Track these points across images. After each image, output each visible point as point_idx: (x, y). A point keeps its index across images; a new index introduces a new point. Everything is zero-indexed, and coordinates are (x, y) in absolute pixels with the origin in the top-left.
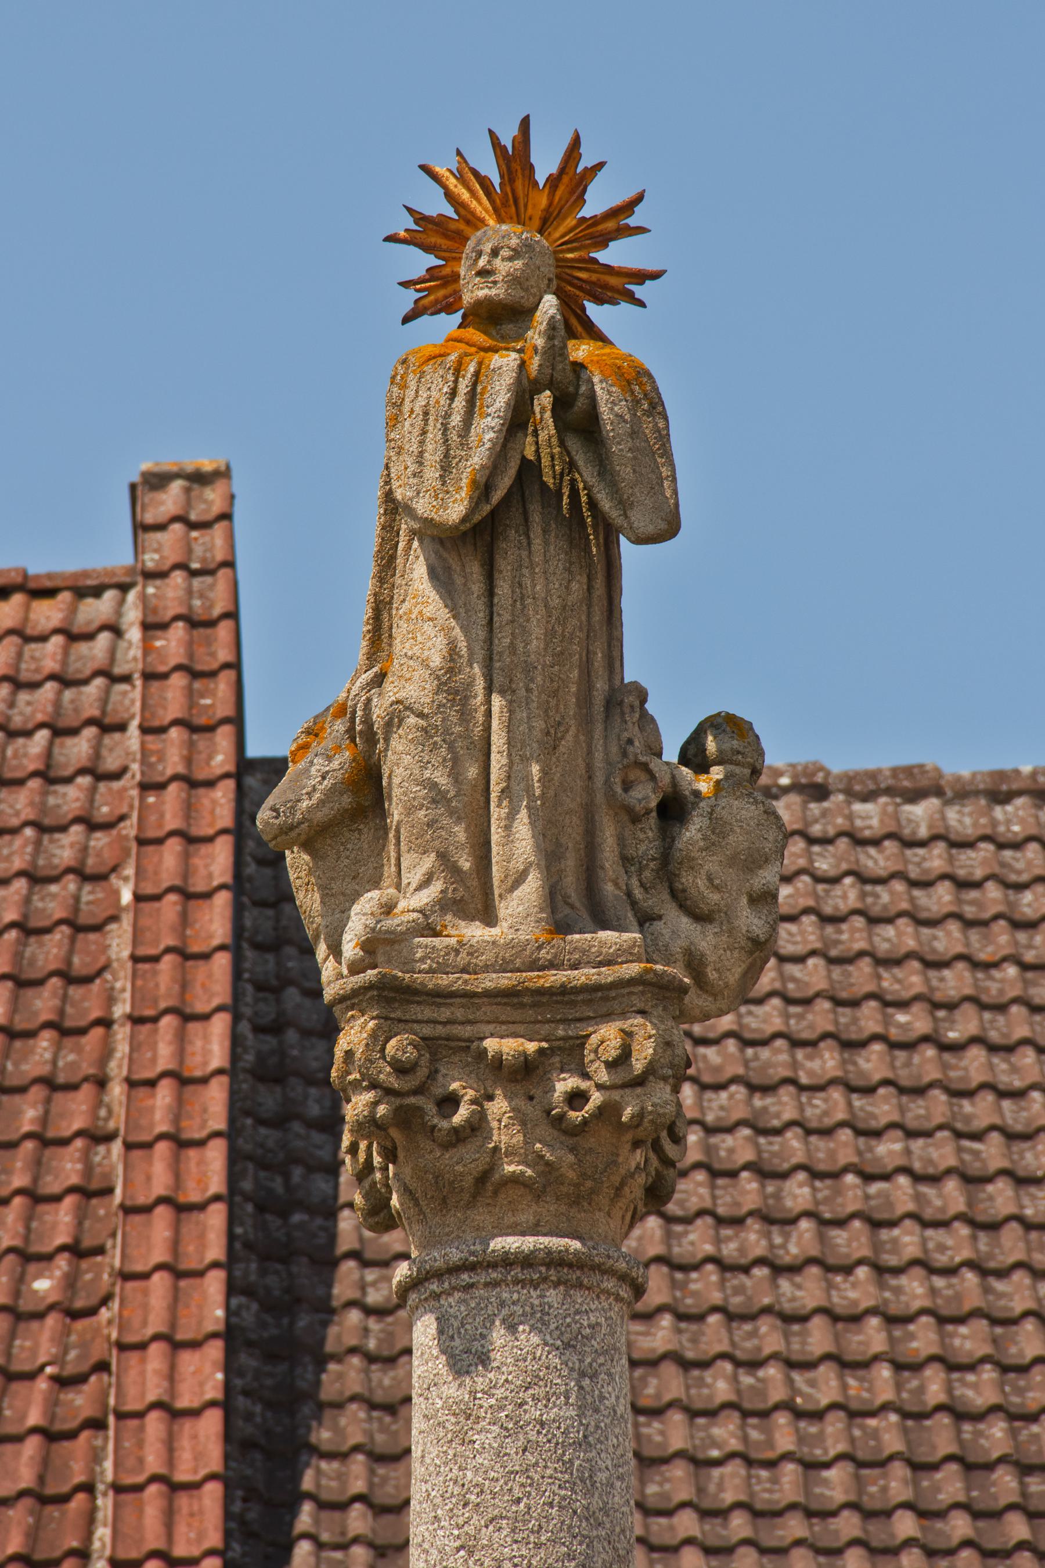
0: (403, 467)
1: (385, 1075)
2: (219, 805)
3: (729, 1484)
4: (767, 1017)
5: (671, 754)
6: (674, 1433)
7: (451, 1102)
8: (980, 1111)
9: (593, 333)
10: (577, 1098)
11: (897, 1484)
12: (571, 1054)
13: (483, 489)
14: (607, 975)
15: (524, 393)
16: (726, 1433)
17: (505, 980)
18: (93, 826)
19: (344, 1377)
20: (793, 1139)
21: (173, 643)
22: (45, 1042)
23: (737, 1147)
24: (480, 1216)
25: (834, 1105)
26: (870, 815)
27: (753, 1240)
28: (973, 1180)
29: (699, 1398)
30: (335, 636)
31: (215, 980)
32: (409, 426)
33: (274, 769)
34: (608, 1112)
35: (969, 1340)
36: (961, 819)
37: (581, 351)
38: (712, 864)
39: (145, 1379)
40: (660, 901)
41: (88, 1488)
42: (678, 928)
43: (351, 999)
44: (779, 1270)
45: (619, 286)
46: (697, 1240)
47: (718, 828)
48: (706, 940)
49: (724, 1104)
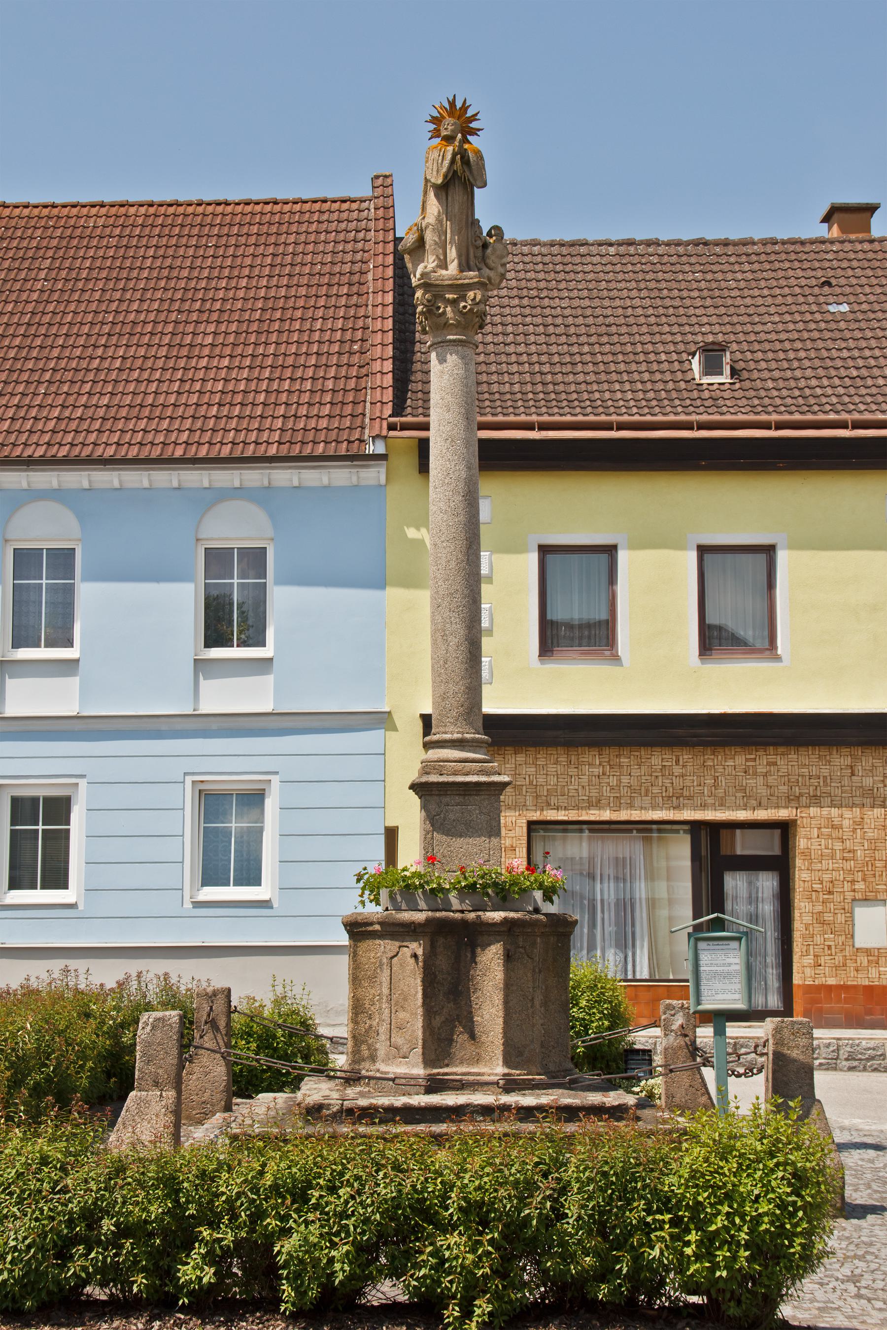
0: (429, 172)
1: (425, 302)
2: (390, 247)
3: (495, 388)
4: (504, 292)
5: (485, 234)
6: (484, 378)
7: (439, 308)
8: (547, 311)
9: (469, 142)
10: (465, 307)
11: (529, 387)
12: (463, 298)
13: (445, 176)
14: (471, 281)
15: (454, 155)
16: (494, 378)
17: (450, 282)
18: (364, 252)
19: (417, 366)
20: (509, 318)
21: (381, 212)
22: (355, 297)
23: (497, 319)
24: (445, 332)
25: (517, 310)
26: (526, 249)
27: (501, 338)
28: (545, 326)
29: (489, 371)
30: (416, 210)
31: (390, 284)
32: (430, 162)
33: (402, 239)
34: (471, 310)
35: (544, 359)
36: (544, 250)
37: (466, 146)
38: (493, 258)
39: (377, 366)
40: (482, 265)
41: (365, 401)
42: (486, 271)
43: (418, 286)
44: (506, 345)
45: (474, 132)
46: (489, 339)
47: (494, 250)
48: (492, 274)
49: (495, 311)
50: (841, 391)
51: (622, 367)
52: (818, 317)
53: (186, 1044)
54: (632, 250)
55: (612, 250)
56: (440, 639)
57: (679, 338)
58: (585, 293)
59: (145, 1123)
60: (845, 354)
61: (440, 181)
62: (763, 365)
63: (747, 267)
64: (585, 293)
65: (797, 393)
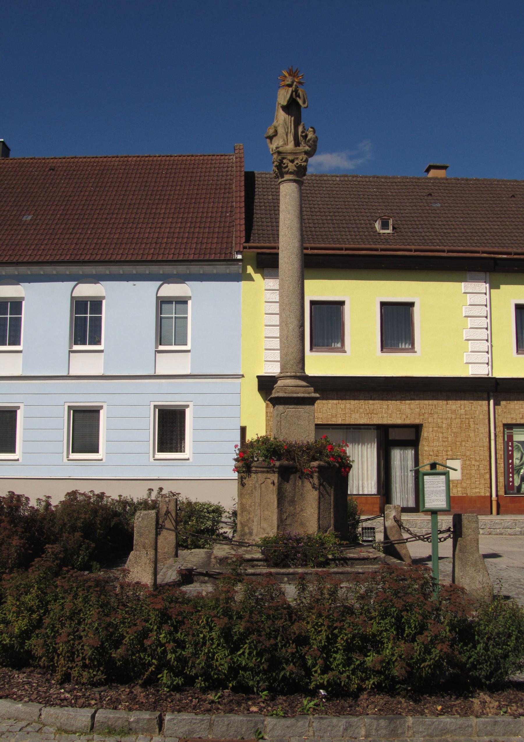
15: (292, 92)
39: (238, 222)
50: (440, 238)
51: (345, 225)
52: (428, 208)
53: (159, 528)
54: (346, 179)
55: (338, 179)
56: (284, 326)
57: (369, 214)
58: (327, 195)
59: (139, 568)
60: (440, 223)
61: (285, 104)
62: (406, 226)
63: (396, 187)
64: (327, 195)
65: (421, 238)
